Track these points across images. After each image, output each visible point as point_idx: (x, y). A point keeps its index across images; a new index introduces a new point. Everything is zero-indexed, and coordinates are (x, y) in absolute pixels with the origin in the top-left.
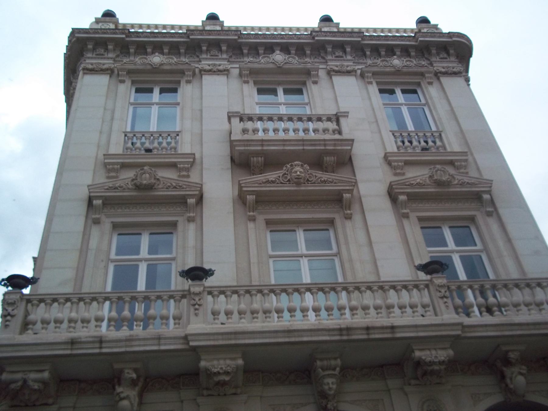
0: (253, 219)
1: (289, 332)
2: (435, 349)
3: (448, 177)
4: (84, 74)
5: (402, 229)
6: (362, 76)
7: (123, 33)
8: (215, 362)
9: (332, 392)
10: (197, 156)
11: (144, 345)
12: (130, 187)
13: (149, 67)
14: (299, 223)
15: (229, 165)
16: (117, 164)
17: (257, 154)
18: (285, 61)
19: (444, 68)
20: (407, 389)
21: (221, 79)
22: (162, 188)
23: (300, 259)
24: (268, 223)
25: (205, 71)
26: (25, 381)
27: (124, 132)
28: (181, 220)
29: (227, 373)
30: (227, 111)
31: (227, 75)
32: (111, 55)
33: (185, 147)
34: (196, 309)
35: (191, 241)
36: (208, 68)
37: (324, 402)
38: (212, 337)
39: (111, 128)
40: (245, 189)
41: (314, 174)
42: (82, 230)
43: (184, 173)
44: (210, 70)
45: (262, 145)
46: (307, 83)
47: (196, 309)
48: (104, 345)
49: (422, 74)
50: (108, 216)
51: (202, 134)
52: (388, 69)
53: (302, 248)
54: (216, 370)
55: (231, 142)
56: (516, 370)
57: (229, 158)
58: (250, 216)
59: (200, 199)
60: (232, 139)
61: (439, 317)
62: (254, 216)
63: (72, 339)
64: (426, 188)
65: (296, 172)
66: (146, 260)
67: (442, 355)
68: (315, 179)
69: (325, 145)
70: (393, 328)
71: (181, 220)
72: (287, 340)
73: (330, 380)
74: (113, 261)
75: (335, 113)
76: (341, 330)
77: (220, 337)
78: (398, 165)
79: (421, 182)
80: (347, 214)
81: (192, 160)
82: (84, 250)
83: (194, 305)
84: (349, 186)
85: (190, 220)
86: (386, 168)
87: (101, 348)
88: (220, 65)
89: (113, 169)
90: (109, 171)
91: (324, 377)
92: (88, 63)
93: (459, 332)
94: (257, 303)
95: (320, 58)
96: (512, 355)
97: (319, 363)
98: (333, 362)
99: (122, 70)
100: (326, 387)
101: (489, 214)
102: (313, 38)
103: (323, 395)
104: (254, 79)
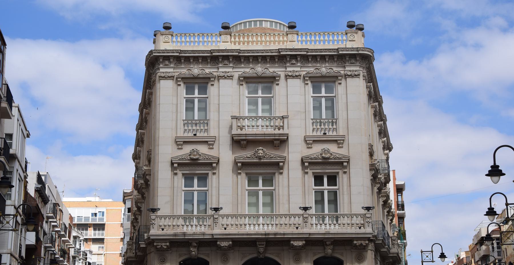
7: (177, 53)
25: (221, 77)
28: (210, 173)
31: (232, 79)
43: (211, 147)
56: (329, 247)
66: (197, 98)
67: (300, 243)
69: (307, 52)
71: (210, 173)
73: (261, 249)
88: (228, 72)
96: (327, 243)
98: (263, 243)
102: (280, 52)
103: (259, 252)
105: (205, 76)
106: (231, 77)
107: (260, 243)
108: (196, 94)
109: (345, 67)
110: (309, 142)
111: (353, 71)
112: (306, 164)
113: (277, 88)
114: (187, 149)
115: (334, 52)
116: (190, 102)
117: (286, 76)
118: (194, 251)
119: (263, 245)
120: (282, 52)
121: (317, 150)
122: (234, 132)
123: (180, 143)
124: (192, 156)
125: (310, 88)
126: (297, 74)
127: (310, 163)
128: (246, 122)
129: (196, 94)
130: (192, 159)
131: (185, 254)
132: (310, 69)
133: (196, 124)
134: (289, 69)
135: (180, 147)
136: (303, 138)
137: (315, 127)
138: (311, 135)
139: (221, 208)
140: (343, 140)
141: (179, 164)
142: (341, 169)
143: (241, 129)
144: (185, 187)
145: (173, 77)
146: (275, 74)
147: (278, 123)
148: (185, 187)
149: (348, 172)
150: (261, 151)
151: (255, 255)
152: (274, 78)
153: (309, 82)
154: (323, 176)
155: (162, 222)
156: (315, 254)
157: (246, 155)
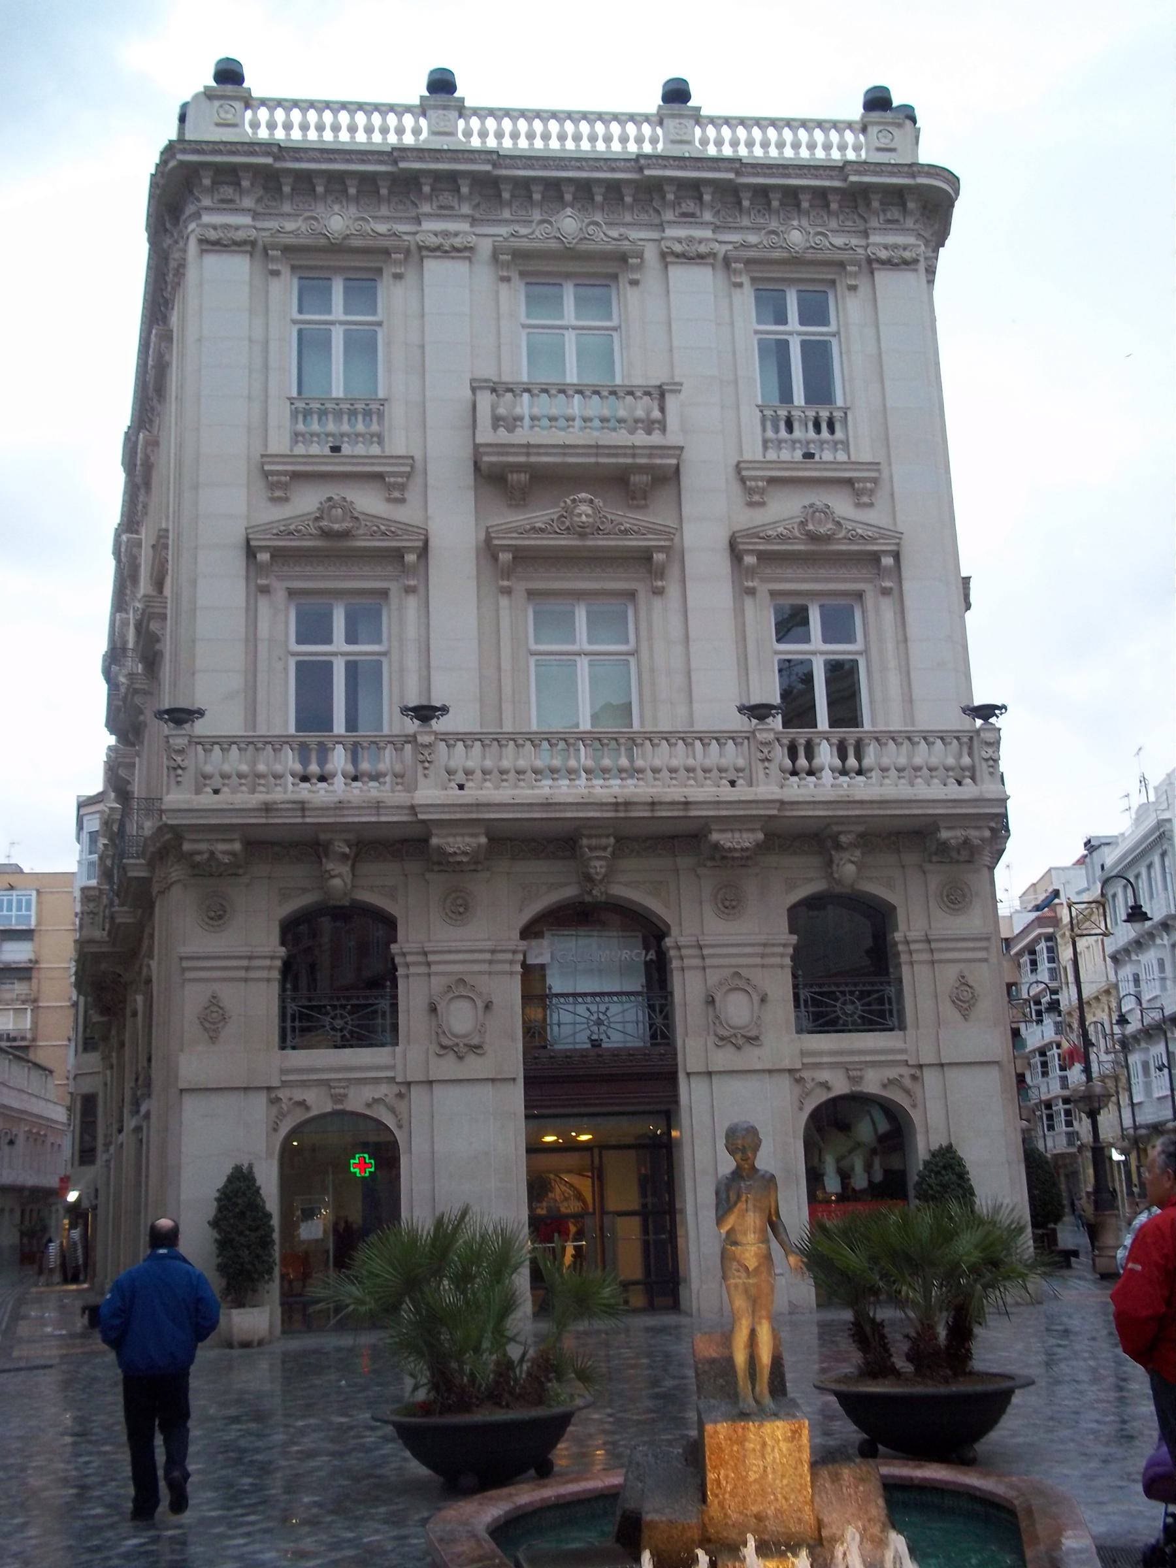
0: (507, 591)
1: (547, 805)
2: (740, 830)
3: (830, 526)
4: (203, 251)
5: (739, 612)
6: (727, 262)
7: (268, 154)
8: (451, 840)
9: (599, 877)
10: (419, 465)
11: (359, 815)
12: (314, 531)
13: (323, 241)
14: (580, 595)
15: (469, 479)
16: (285, 473)
17: (518, 468)
18: (582, 236)
19: (886, 248)
20: (928, 867)
21: (456, 269)
22: (364, 535)
23: (577, 658)
24: (531, 594)
25: (428, 248)
26: (212, 853)
27: (289, 399)
28: (394, 587)
29: (465, 853)
30: (468, 376)
31: (469, 259)
32: (248, 202)
33: (398, 444)
34: (426, 768)
35: (412, 631)
36: (433, 241)
37: (589, 885)
38: (446, 809)
39: (266, 390)
40: (496, 542)
41: (609, 517)
42: (244, 605)
43: (396, 494)
44: (438, 248)
45: (528, 454)
46: (621, 279)
47: (426, 768)
48: (307, 813)
49: (842, 265)
50: (280, 578)
51: (424, 403)
52: (777, 254)
53: (582, 642)
54: (451, 850)
55: (476, 446)
56: (846, 855)
57: (471, 464)
58: (502, 587)
59: (424, 551)
60: (479, 440)
61: (753, 789)
62: (509, 587)
63: (266, 804)
64: (792, 544)
65: (580, 515)
66: (342, 323)
67: (747, 839)
68: (611, 526)
70: (687, 804)
71: (394, 587)
72: (544, 815)
73: (598, 863)
74: (294, 654)
75: (658, 383)
76: (617, 804)
77: (458, 809)
78: (757, 487)
79: (785, 532)
80: (657, 587)
81: (408, 469)
82: (252, 639)
83: (422, 762)
84: (665, 540)
85: (410, 590)
86: (736, 488)
87: (303, 817)
88: (456, 234)
89: (279, 482)
90: (272, 486)
91: (590, 859)
92: (207, 226)
93: (775, 812)
94: (509, 758)
95: (651, 212)
96: (843, 839)
97: (585, 842)
98: (604, 841)
99: (274, 247)
100: (592, 871)
101: (886, 592)
102: (641, 169)
103: (589, 878)
104: (521, 268)
105: (370, 243)
106: (464, 252)
107: (594, 842)
108: (338, 310)
109: (866, 234)
110: (754, 485)
111: (895, 247)
112: (750, 560)
113: (632, 294)
114: (306, 502)
115: (831, 178)
116: (311, 343)
117: (663, 255)
118: (340, 879)
119: (605, 849)
120: (649, 167)
121: (784, 509)
122: (485, 435)
123: (279, 480)
124: (324, 523)
125: (746, 299)
126: (703, 249)
127: (762, 556)
128: (524, 405)
129: (338, 310)
130: (326, 534)
131: (304, 890)
132: (749, 235)
133: (338, 415)
134: (671, 232)
135: (278, 493)
136: (731, 471)
137: (770, 434)
138: (761, 458)
139: (444, 710)
140: (875, 481)
141: (278, 554)
142: (870, 581)
143: (511, 429)
144: (298, 642)
145: (253, 243)
146: (626, 246)
147: (642, 408)
148: (298, 642)
149: (896, 592)
150: (584, 508)
151: (569, 892)
152: (622, 258)
153: (745, 279)
154: (805, 609)
155: (215, 762)
156: (791, 885)
157: (537, 518)
